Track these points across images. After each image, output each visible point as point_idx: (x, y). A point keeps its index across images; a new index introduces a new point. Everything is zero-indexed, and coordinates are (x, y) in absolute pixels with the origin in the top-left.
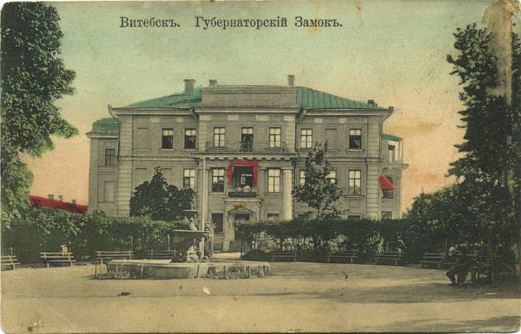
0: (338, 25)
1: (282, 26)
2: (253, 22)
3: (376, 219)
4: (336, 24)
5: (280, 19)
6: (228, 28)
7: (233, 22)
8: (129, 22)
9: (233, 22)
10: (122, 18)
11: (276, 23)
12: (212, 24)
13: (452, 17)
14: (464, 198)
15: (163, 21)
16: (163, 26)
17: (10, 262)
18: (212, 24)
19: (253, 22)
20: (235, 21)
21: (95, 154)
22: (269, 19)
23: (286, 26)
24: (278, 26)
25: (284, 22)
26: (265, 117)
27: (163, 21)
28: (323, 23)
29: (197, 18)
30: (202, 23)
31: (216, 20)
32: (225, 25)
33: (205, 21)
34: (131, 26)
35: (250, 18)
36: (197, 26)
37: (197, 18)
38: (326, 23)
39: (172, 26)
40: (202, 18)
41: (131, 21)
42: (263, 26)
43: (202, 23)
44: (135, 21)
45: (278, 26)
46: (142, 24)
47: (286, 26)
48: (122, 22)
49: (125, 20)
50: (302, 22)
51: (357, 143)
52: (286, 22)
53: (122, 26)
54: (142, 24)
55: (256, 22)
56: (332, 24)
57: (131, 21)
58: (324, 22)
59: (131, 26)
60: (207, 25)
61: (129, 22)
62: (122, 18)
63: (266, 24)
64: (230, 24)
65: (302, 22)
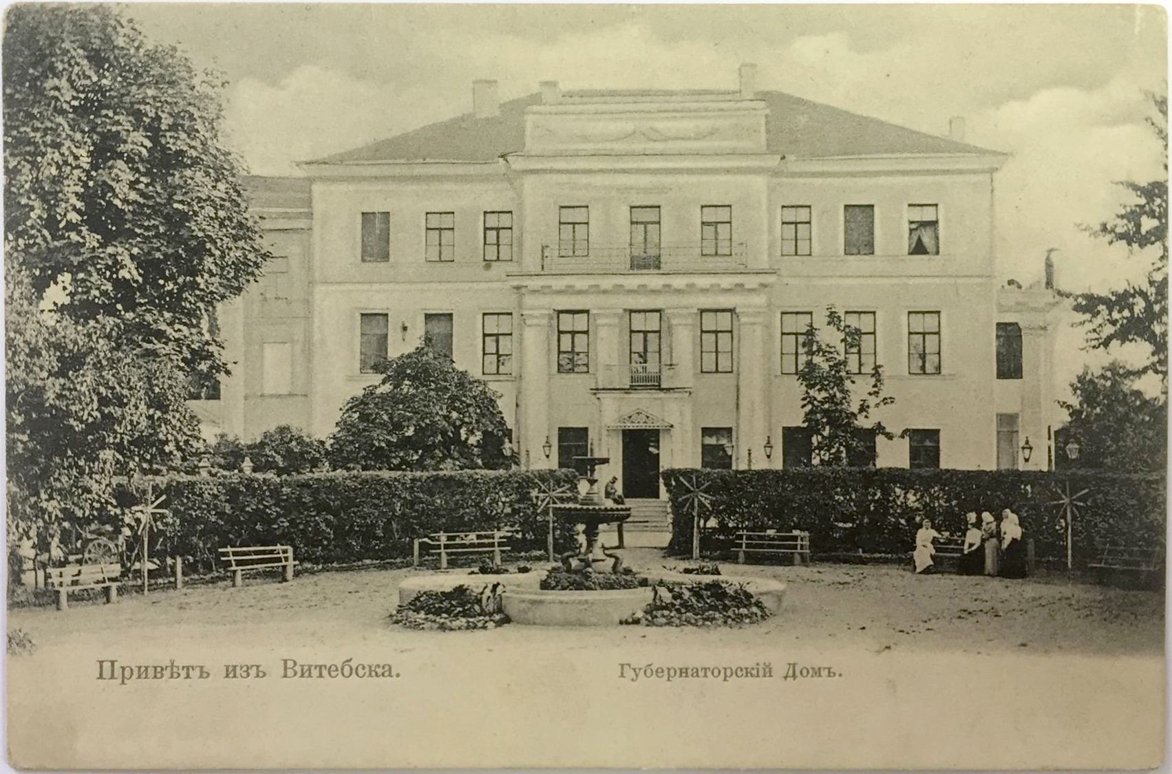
1: (310, 666)
4: (830, 673)
8: (298, 669)
10: (285, 661)
11: (754, 672)
16: (370, 675)
17: (235, 554)
25: (768, 671)
26: (798, 170)
29: (622, 665)
30: (629, 673)
31: (654, 669)
34: (302, 676)
35: (711, 665)
36: (622, 675)
37: (622, 665)
38: (370, 670)
39: (201, 676)
41: (302, 666)
43: (629, 673)
46: (325, 673)
47: (227, 667)
48: (286, 668)
49: (290, 664)
50: (288, 668)
51: (927, 240)
53: (285, 676)
57: (123, 669)
59: (302, 676)
62: (101, 662)
63: (361, 672)
65: (288, 668)
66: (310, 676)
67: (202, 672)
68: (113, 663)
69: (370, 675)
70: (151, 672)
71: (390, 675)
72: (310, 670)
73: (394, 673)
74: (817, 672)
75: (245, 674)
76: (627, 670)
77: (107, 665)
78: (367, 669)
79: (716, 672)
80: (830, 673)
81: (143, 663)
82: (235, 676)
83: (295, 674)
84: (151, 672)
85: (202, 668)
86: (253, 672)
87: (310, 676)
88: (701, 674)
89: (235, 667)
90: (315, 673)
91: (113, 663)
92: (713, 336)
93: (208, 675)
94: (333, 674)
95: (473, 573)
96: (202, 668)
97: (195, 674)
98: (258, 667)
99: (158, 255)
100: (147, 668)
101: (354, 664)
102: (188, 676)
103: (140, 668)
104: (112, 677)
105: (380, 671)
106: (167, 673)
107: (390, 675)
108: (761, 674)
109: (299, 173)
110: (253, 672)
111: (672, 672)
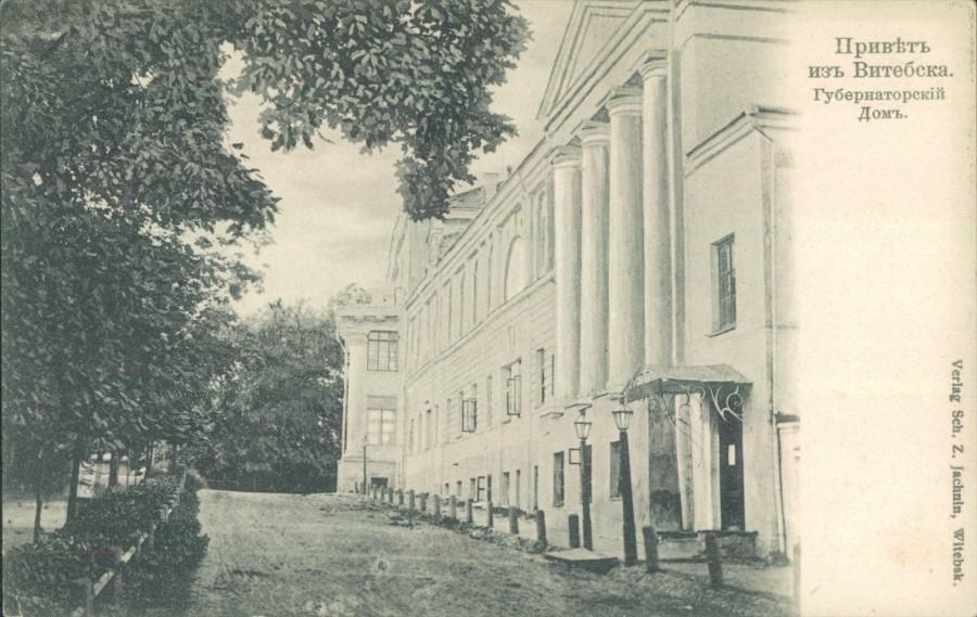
3: (223, 134)
5: (935, 90)
8: (868, 70)
11: (929, 96)
13: (427, 402)
15: (929, 67)
16: (929, 75)
22: (920, 90)
23: (811, 68)
27: (929, 67)
28: (865, 47)
30: (823, 97)
31: (844, 92)
32: (858, 51)
33: (827, 93)
36: (817, 99)
37: (817, 91)
38: (929, 71)
39: (923, 51)
42: (915, 74)
43: (823, 97)
44: (878, 68)
46: (891, 73)
48: (857, 70)
49: (861, 66)
54: (891, 73)
57: (858, 45)
58: (868, 46)
61: (868, 70)
63: (921, 72)
64: (868, 50)
66: (878, 76)
67: (923, 47)
68: (849, 40)
69: (929, 75)
70: (881, 47)
71: (946, 75)
72: (872, 73)
73: (948, 73)
75: (826, 74)
77: (844, 42)
79: (897, 96)
81: (874, 40)
82: (818, 76)
83: (866, 74)
84: (881, 47)
85: (923, 44)
86: (893, 115)
87: (878, 76)
88: (885, 97)
89: (818, 69)
90: (883, 73)
91: (849, 40)
93: (929, 50)
94: (898, 74)
96: (923, 44)
97: (893, 115)
99: (152, 325)
100: (877, 44)
101: (915, 66)
102: (912, 51)
103: (867, 93)
104: (849, 52)
105: (937, 71)
106: (895, 48)
107: (946, 75)
108: (935, 95)
109: (599, 107)
110: (833, 73)
111: (859, 96)
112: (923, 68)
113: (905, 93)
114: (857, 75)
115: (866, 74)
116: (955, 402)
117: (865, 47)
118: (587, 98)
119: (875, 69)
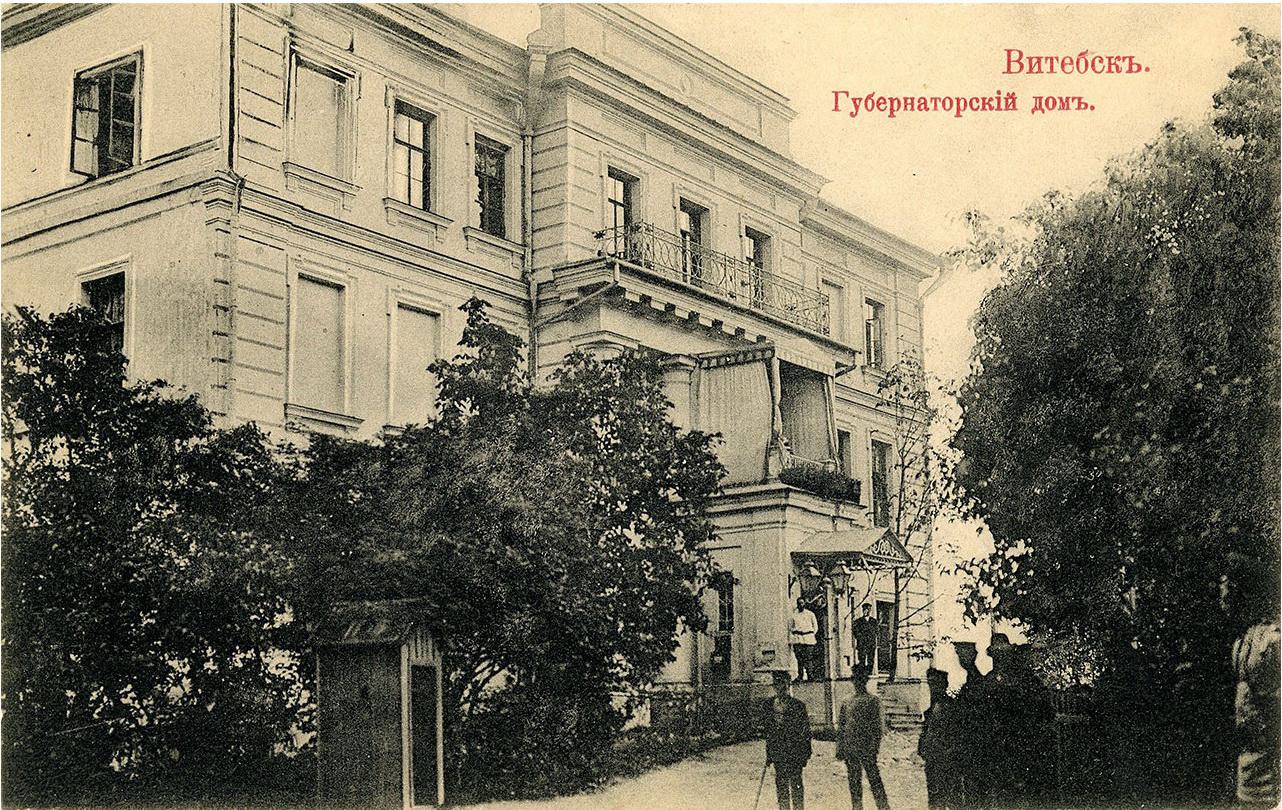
0: (1086, 105)
1: (1039, 59)
2: (947, 101)
5: (1003, 95)
6: (900, 113)
7: (909, 107)
9: (909, 107)
10: (1009, 52)
11: (994, 103)
12: (866, 106)
14: (102, 459)
15: (984, 99)
16: (1110, 71)
18: (866, 106)
19: (947, 101)
20: (912, 99)
21: (985, 344)
24: (999, 109)
27: (984, 99)
28: (899, 102)
29: (836, 93)
31: (875, 98)
33: (854, 100)
34: (1031, 71)
36: (836, 109)
37: (836, 93)
38: (984, 104)
39: (1130, 71)
40: (847, 93)
43: (846, 104)
44: (1039, 59)
45: (999, 109)
46: (940, 105)
48: (1009, 61)
49: (1015, 56)
52: (1014, 102)
54: (1057, 66)
55: (955, 102)
56: (1125, 66)
57: (1030, 59)
58: (902, 101)
60: (857, 107)
62: (1009, 52)
63: (1099, 67)
66: (1040, 71)
67: (1080, 103)
69: (1110, 71)
74: (1065, 104)
76: (843, 100)
78: (1106, 61)
80: (1081, 104)
83: (1022, 66)
86: (1074, 105)
90: (1046, 67)
92: (613, 226)
95: (5, 510)
97: (1074, 105)
98: (1131, 58)
103: (906, 99)
108: (1003, 106)
111: (962, 102)
112: (1101, 61)
113: (958, 100)
114: (1009, 71)
115: (1022, 66)
116: (1032, 103)
117: (899, 102)
118: (32, 238)
119: (1034, 61)
